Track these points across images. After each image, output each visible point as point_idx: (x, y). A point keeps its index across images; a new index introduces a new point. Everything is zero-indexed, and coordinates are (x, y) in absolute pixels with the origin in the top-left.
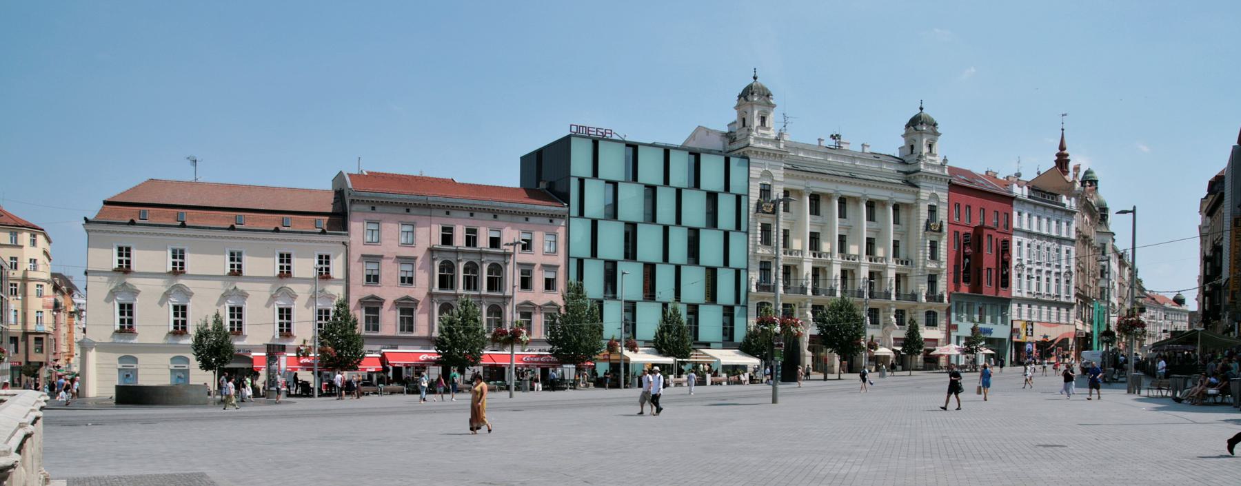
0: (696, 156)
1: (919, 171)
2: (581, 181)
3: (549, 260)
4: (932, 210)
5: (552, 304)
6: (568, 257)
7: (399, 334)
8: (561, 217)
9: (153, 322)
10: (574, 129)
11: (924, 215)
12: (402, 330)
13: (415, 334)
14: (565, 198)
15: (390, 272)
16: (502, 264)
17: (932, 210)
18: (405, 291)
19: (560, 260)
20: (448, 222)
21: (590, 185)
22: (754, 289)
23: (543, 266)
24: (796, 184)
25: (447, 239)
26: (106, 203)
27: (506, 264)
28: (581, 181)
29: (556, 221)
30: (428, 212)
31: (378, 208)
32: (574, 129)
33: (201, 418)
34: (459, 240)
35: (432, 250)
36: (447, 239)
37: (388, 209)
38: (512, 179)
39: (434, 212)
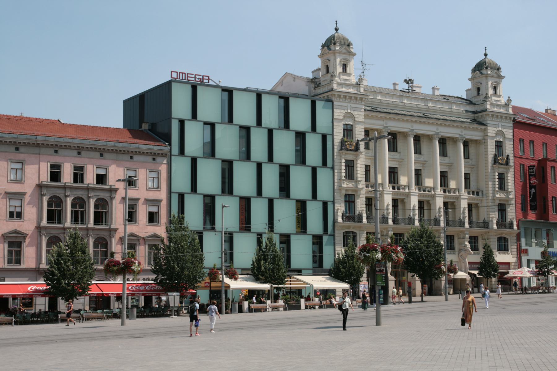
0: (285, 99)
1: (485, 110)
2: (182, 123)
3: (152, 195)
4: (499, 145)
6: (170, 192)
7: (6, 266)
11: (492, 150)
12: (9, 262)
13: (23, 266)
14: (167, 138)
16: (108, 199)
17: (499, 145)
19: (162, 195)
20: (56, 160)
22: (340, 220)
23: (147, 200)
24: (376, 124)
25: (55, 175)
27: (112, 199)
28: (182, 123)
29: (159, 159)
30: (37, 150)
31: (22, 149)
32: (174, 75)
34: (67, 177)
36: (55, 175)
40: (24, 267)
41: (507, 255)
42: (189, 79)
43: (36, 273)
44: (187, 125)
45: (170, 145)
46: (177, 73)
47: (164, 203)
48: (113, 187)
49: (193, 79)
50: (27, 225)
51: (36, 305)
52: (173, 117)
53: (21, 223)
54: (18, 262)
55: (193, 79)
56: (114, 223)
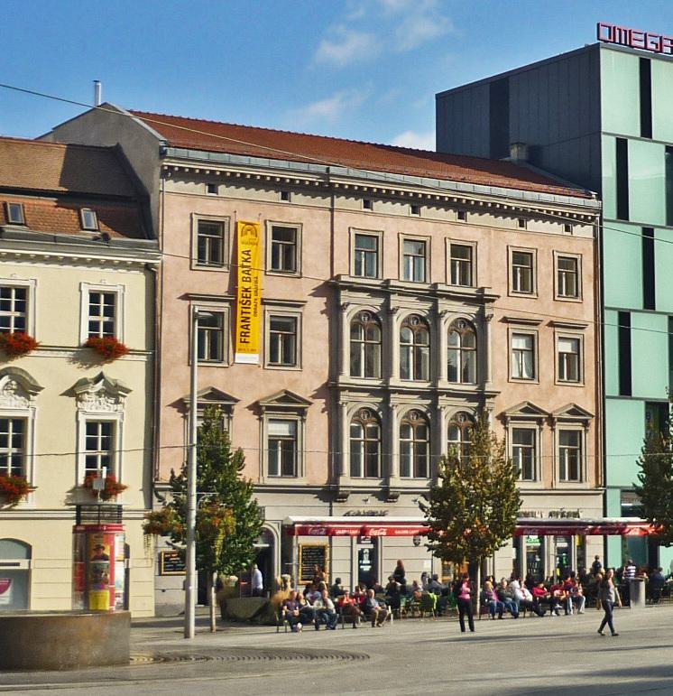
2: (622, 145)
3: (564, 312)
5: (576, 411)
12: (272, 471)
13: (299, 481)
14: (591, 184)
21: (636, 150)
23: (551, 324)
28: (622, 145)
32: (605, 34)
40: (304, 483)
41: (64, 497)
42: (634, 43)
43: (569, 541)
44: (632, 147)
45: (599, 197)
46: (610, 28)
47: (589, 332)
48: (486, 292)
49: (642, 44)
50: (308, 376)
51: (331, 560)
52: (671, 65)
53: (296, 375)
54: (289, 470)
55: (642, 44)
56: (490, 379)
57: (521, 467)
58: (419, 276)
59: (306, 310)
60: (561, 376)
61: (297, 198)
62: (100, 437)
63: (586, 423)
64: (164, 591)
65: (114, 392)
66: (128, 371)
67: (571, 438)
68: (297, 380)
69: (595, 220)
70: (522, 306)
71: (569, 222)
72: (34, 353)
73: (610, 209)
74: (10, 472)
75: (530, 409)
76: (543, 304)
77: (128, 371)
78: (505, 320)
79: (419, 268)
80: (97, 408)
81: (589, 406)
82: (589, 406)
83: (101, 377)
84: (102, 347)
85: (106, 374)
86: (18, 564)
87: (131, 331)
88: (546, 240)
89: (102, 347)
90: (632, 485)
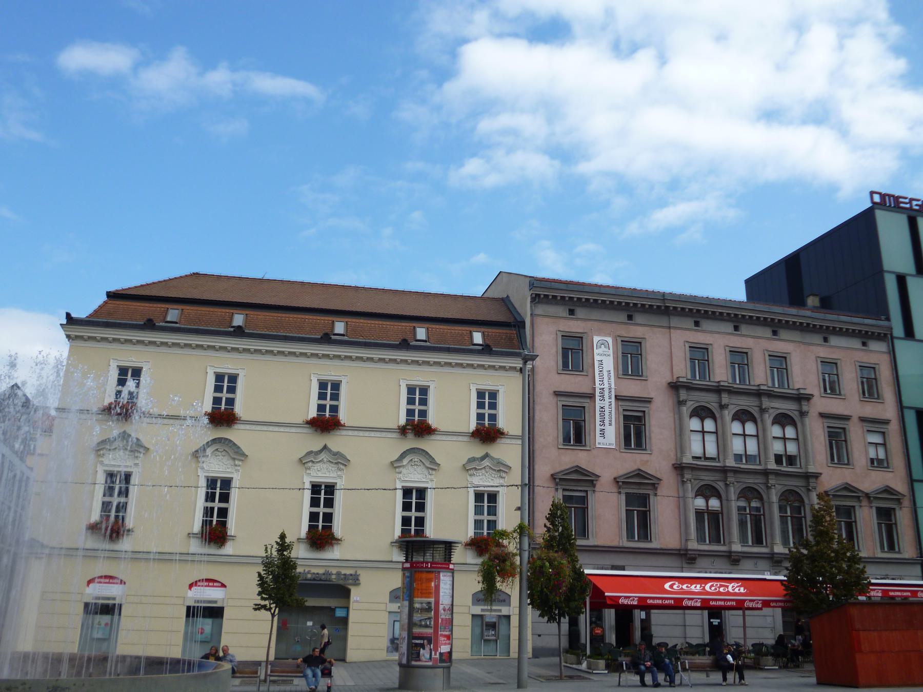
2: (901, 280)
3: (870, 410)
5: (888, 490)
6: (901, 407)
8: (880, 337)
9: (166, 514)
10: (877, 198)
12: (630, 536)
13: (654, 545)
14: (882, 311)
15: (606, 433)
18: (631, 461)
19: (888, 410)
23: (863, 420)
26: (111, 295)
28: (901, 280)
30: (664, 321)
32: (877, 198)
33: (205, 602)
35: (675, 387)
37: (596, 314)
38: (740, 295)
39: (675, 321)
45: (888, 319)
47: (894, 427)
54: (645, 534)
57: (844, 536)
58: (783, 383)
59: (654, 406)
60: (832, 459)
61: (639, 318)
62: (322, 496)
63: (899, 501)
64: (539, 636)
65: (501, 468)
66: (509, 452)
67: (886, 515)
68: (647, 461)
69: (886, 337)
70: (834, 406)
71: (865, 337)
72: (504, 441)
73: (898, 329)
74: (320, 527)
75: (847, 488)
76: (850, 404)
77: (509, 452)
78: (823, 415)
79: (744, 375)
80: (485, 481)
81: (900, 486)
82: (900, 486)
83: (487, 456)
84: (487, 434)
85: (329, 446)
86: (500, 611)
87: (509, 417)
88: (849, 355)
89: (487, 434)
90: (131, 527)
